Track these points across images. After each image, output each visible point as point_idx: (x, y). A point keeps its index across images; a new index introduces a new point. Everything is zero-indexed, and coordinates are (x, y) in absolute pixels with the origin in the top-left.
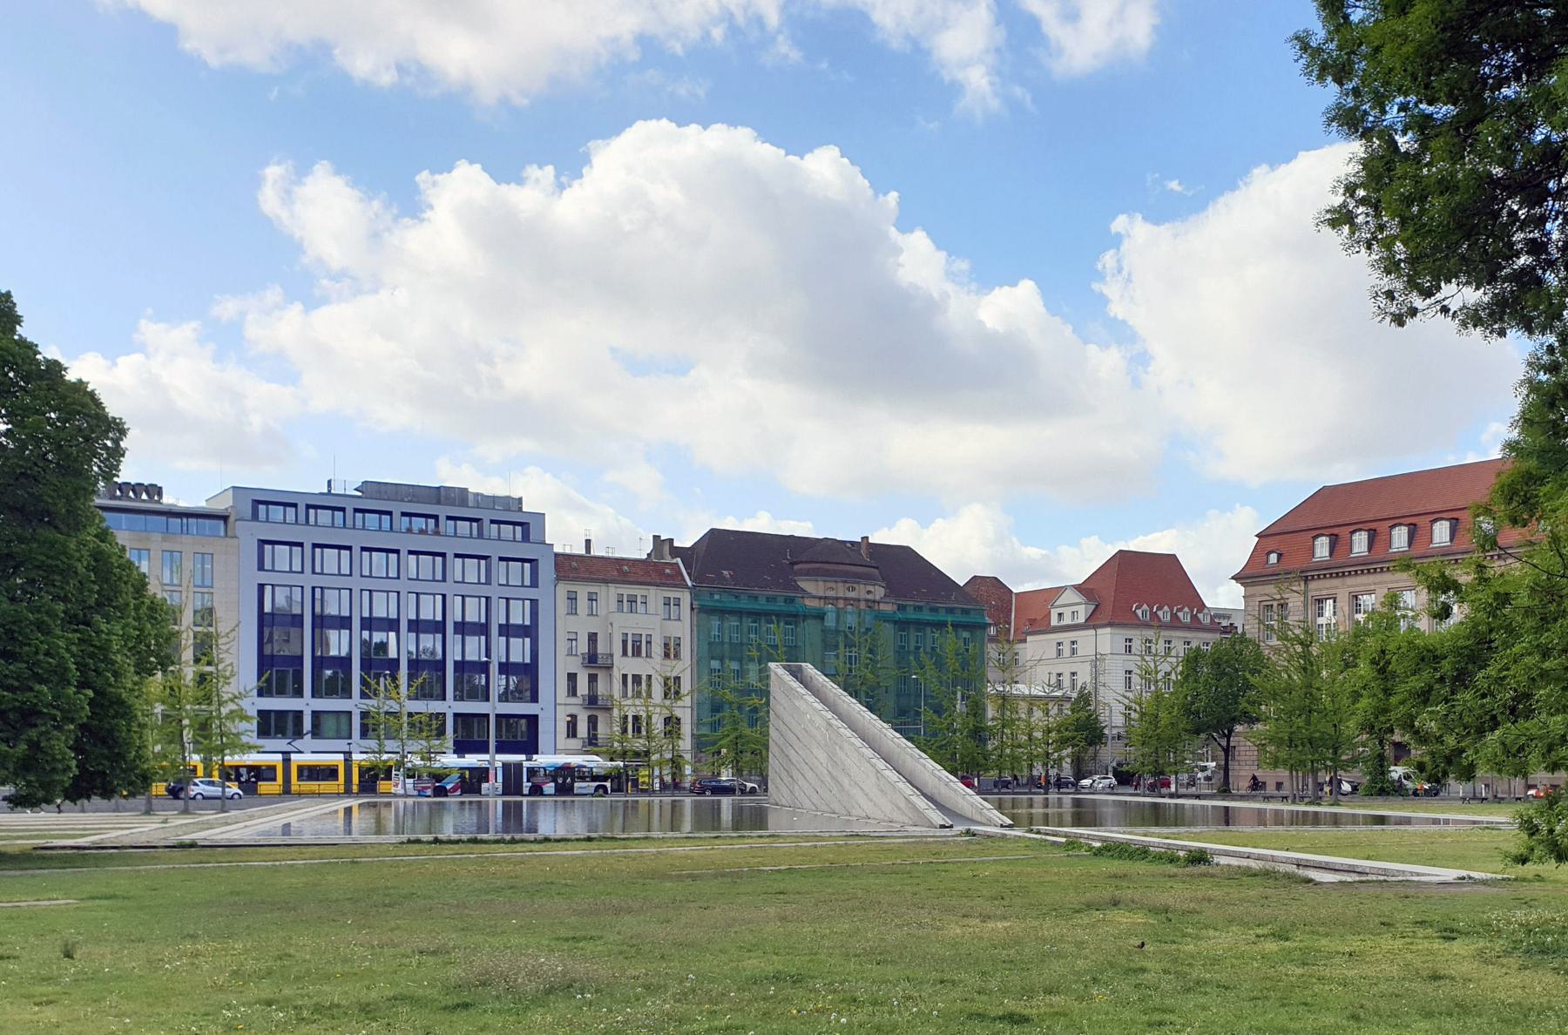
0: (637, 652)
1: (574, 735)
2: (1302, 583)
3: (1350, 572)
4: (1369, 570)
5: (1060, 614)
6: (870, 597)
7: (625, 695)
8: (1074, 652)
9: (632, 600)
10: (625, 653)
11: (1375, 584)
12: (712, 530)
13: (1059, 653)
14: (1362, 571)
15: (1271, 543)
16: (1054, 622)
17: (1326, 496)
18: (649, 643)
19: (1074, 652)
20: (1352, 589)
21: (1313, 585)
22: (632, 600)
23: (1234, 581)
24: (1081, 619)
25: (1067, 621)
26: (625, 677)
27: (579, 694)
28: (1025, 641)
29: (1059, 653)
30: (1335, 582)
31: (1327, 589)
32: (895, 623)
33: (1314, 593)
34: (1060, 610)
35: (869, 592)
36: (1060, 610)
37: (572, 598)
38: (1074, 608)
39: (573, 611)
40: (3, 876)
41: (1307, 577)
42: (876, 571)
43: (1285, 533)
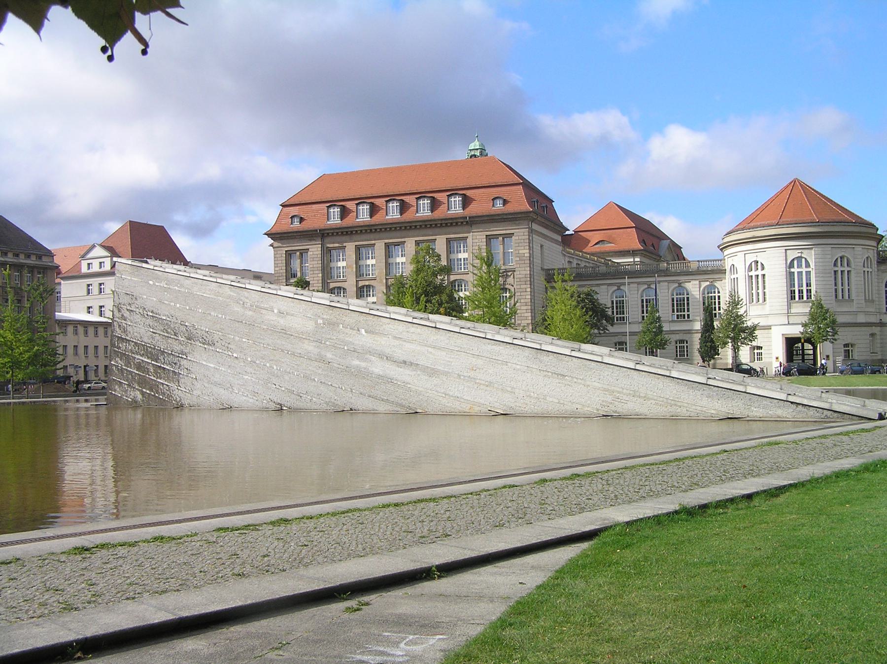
5: (89, 264)
12: (162, 228)
15: (294, 211)
21: (327, 240)
25: (95, 268)
34: (89, 261)
36: (89, 261)
38: (101, 260)
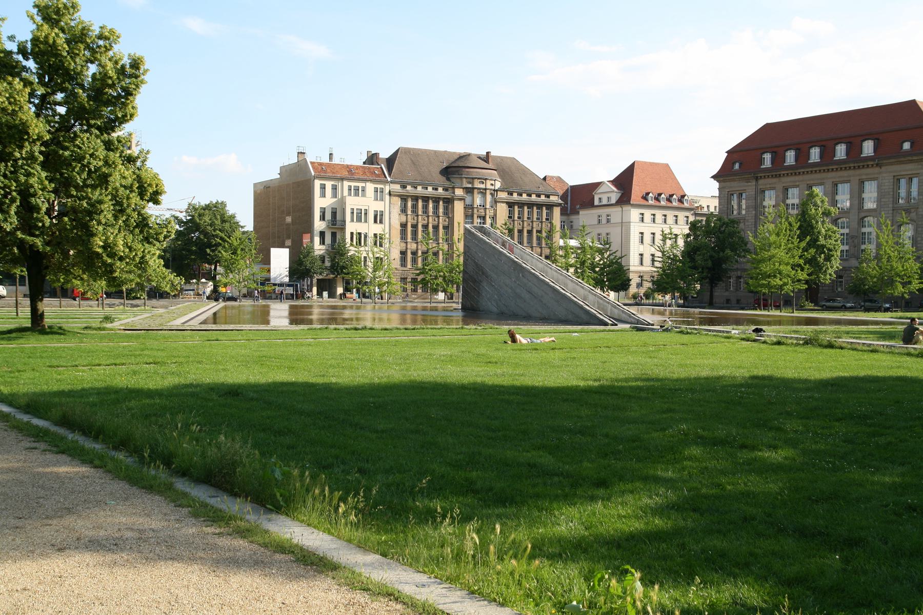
0: (359, 220)
1: (324, 219)
2: (754, 181)
3: (784, 174)
4: (828, 170)
5: (600, 199)
6: (493, 188)
7: (352, 245)
8: (608, 221)
9: (357, 189)
10: (352, 220)
11: (799, 181)
13: (599, 221)
14: (788, 174)
16: (596, 203)
17: (769, 130)
18: (366, 214)
19: (608, 221)
20: (784, 185)
21: (761, 182)
22: (357, 189)
23: (712, 179)
24: (613, 201)
25: (605, 202)
26: (352, 234)
27: (326, 219)
28: (578, 213)
29: (599, 221)
30: (774, 180)
31: (770, 184)
32: (507, 203)
33: (761, 187)
34: (600, 196)
35: (492, 185)
36: (600, 196)
37: (323, 187)
38: (609, 195)
39: (323, 195)
40: (3, 339)
41: (757, 177)
42: (495, 172)
43: (916, 128)
